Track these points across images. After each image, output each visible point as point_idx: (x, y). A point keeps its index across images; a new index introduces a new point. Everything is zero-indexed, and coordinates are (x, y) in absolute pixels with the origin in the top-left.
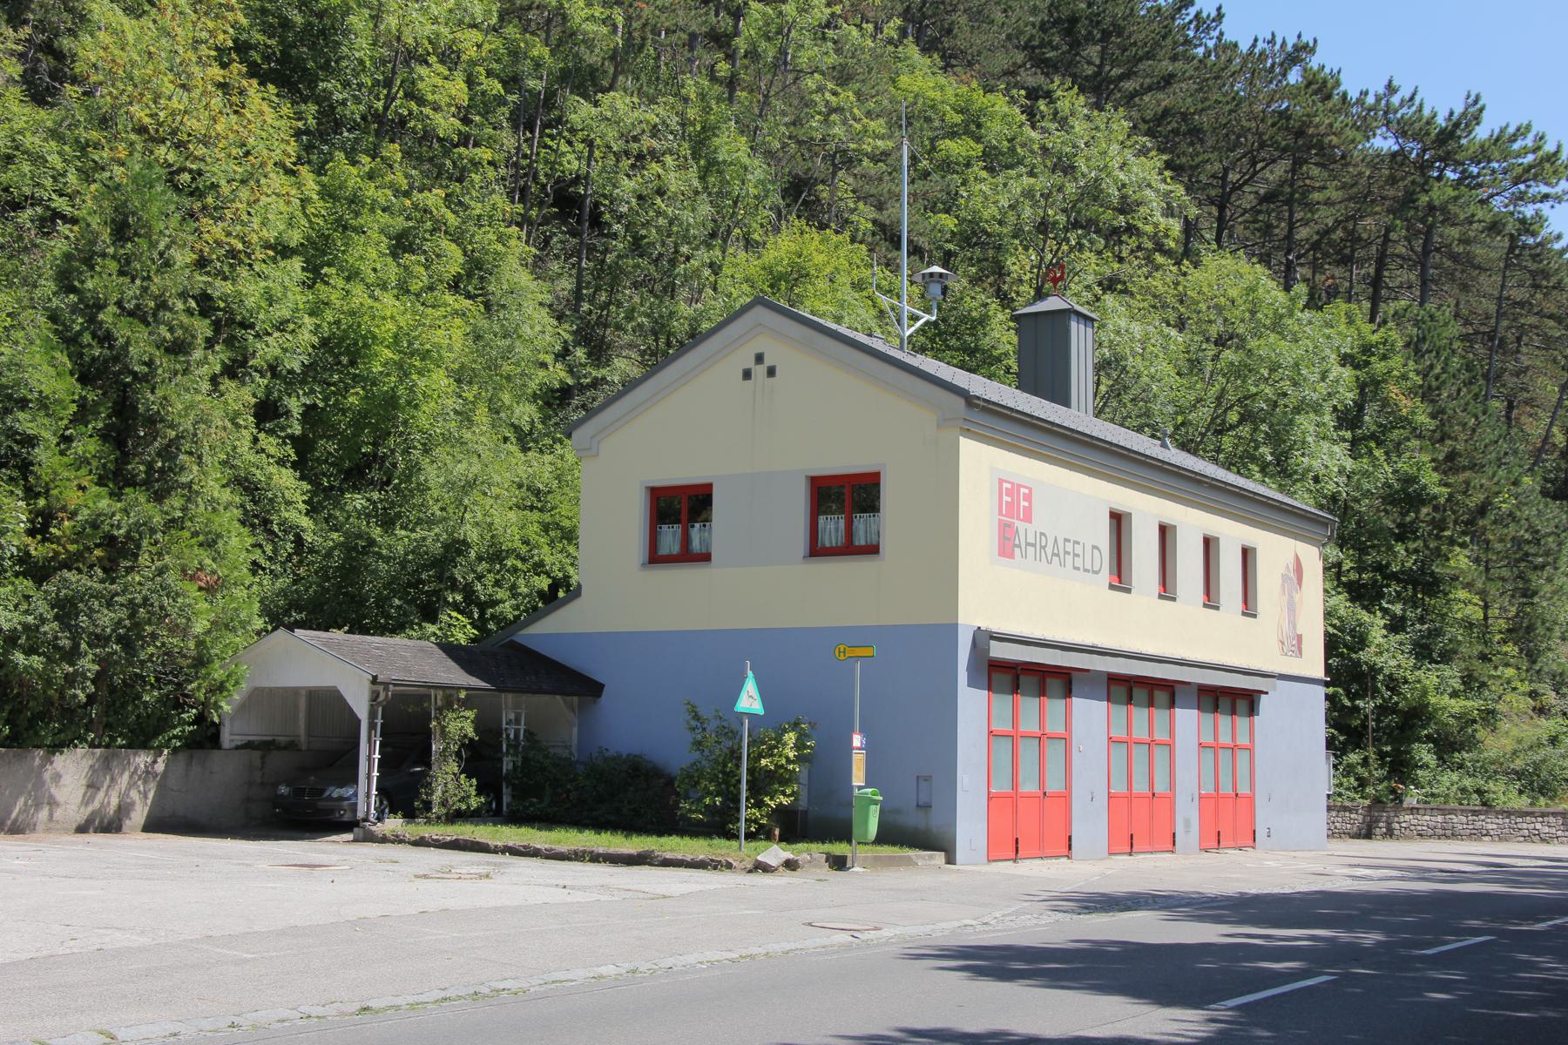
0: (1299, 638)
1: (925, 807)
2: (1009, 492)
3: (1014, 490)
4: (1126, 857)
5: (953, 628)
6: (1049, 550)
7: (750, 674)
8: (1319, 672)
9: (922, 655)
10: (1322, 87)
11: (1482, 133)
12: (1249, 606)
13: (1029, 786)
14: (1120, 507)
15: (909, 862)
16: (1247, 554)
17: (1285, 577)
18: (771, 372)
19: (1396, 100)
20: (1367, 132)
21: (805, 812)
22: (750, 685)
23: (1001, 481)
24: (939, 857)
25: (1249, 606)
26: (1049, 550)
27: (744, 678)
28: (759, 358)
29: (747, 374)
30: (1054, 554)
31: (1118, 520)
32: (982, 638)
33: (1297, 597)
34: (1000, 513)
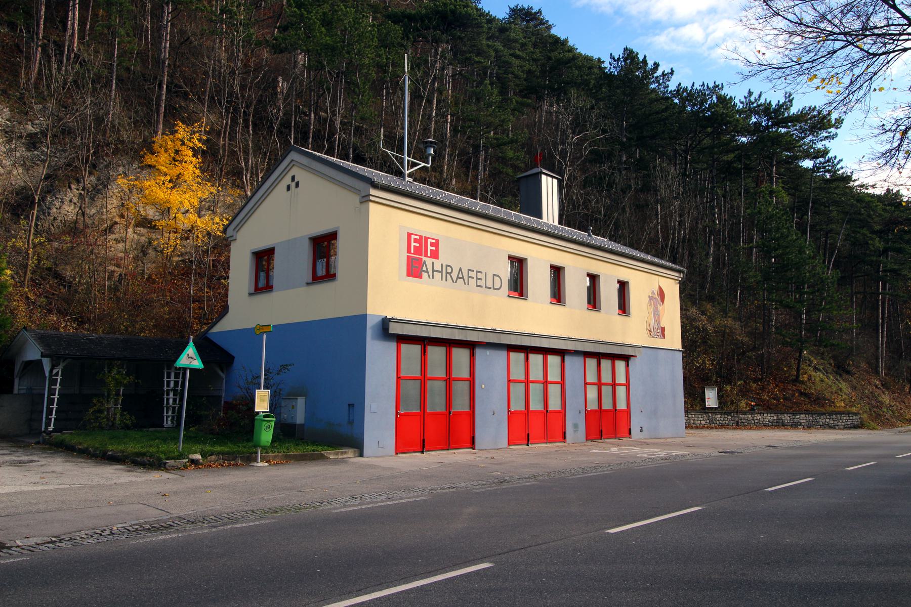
0: (663, 329)
1: (351, 422)
2: (415, 241)
3: (422, 240)
4: (418, 454)
5: (364, 316)
6: (454, 275)
7: (191, 344)
8: (678, 345)
9: (349, 334)
10: (724, 101)
11: (794, 110)
12: (624, 307)
13: (536, 405)
14: (593, 271)
15: (321, 458)
16: (623, 286)
17: (651, 298)
18: (297, 185)
19: (752, 99)
20: (749, 117)
21: (302, 425)
22: (191, 350)
23: (409, 235)
24: (350, 453)
25: (624, 307)
26: (454, 275)
27: (184, 346)
28: (293, 178)
29: (289, 188)
30: (458, 277)
31: (593, 278)
32: (385, 323)
33: (660, 308)
34: (409, 251)
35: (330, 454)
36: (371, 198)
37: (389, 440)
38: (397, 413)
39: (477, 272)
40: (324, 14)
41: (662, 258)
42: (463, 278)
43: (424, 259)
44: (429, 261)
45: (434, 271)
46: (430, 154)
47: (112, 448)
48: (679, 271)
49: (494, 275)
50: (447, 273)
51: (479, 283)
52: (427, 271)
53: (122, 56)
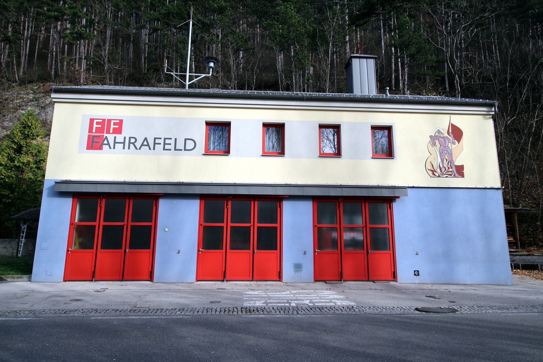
6: (138, 145)
34: (90, 130)
35: (8, 278)
36: (54, 100)
37: (60, 270)
38: (68, 251)
39: (165, 139)
40: (14, 7)
41: (142, 86)
42: (148, 145)
43: (105, 135)
44: (111, 137)
45: (115, 143)
46: (211, 67)
47: (385, 333)
48: (490, 106)
49: (186, 140)
50: (130, 143)
51: (167, 147)
52: (108, 144)
53: (200, 70)
